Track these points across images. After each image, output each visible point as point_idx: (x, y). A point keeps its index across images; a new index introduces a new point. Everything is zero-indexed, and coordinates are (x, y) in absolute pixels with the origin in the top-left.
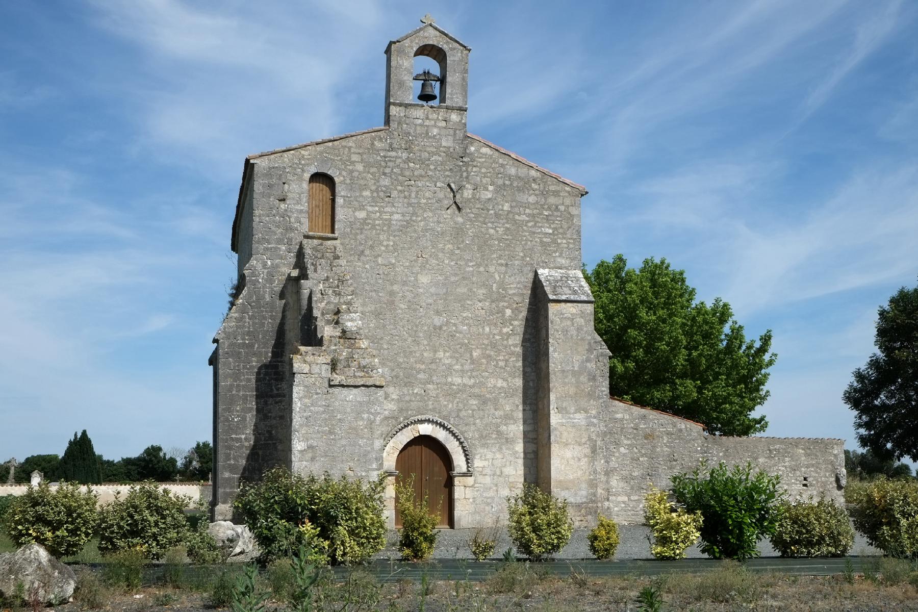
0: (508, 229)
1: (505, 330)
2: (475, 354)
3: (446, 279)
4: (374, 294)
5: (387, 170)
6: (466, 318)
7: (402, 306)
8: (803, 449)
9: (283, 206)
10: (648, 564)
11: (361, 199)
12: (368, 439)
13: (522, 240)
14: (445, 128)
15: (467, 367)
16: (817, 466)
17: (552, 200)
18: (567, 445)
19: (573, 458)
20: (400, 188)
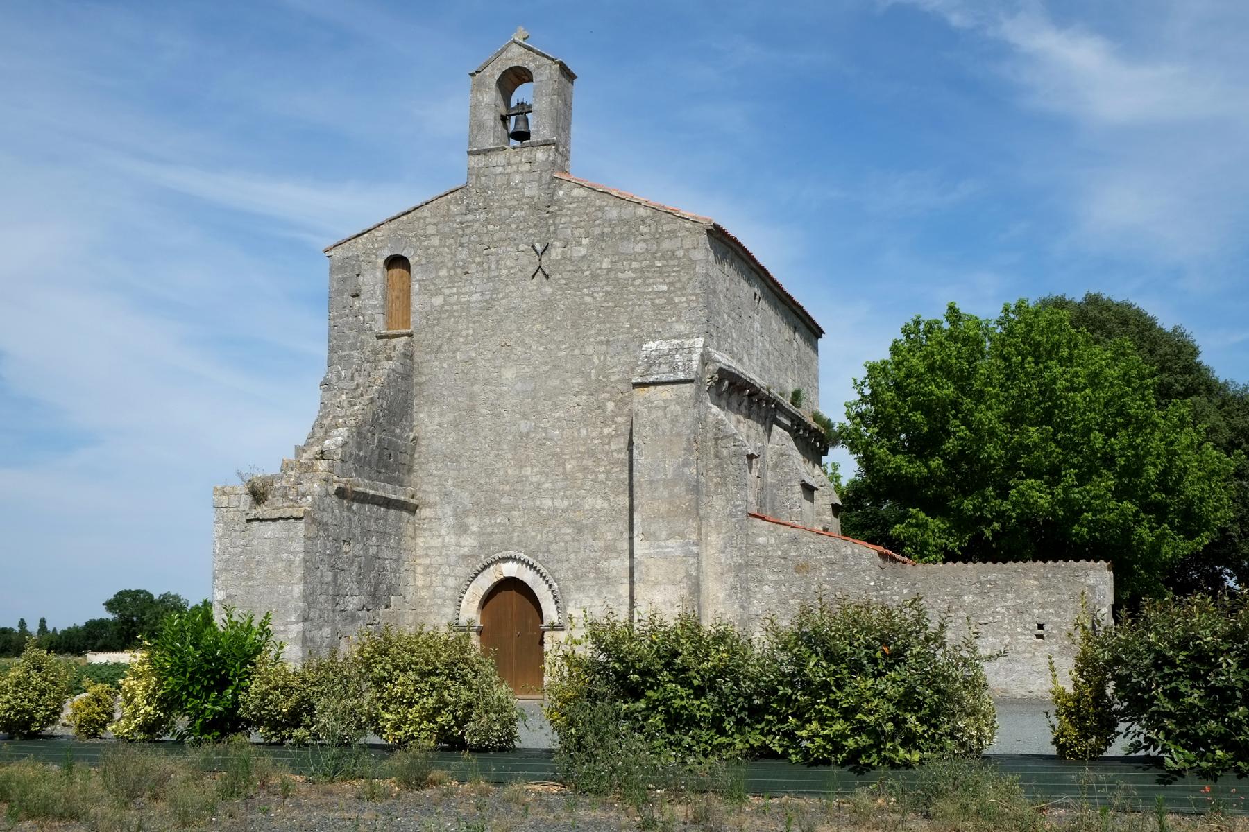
0: (608, 293)
1: (606, 431)
2: (568, 467)
3: (535, 369)
4: (452, 399)
5: (465, 240)
6: (559, 419)
7: (484, 412)
8: (1036, 579)
9: (357, 303)
10: (1048, 764)
11: (437, 281)
12: (287, 585)
13: (627, 305)
14: (529, 172)
15: (559, 484)
16: (1059, 604)
17: (667, 245)
18: (656, 584)
19: (665, 603)
20: (478, 259)
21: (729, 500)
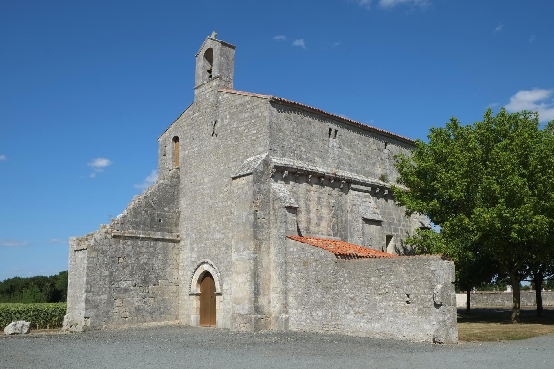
0: (236, 138)
4: (190, 194)
5: (193, 125)
6: (221, 198)
8: (405, 267)
9: (165, 158)
19: (242, 283)
21: (278, 230)
